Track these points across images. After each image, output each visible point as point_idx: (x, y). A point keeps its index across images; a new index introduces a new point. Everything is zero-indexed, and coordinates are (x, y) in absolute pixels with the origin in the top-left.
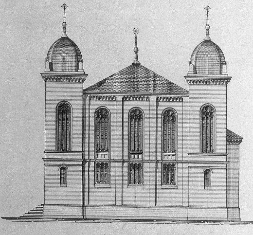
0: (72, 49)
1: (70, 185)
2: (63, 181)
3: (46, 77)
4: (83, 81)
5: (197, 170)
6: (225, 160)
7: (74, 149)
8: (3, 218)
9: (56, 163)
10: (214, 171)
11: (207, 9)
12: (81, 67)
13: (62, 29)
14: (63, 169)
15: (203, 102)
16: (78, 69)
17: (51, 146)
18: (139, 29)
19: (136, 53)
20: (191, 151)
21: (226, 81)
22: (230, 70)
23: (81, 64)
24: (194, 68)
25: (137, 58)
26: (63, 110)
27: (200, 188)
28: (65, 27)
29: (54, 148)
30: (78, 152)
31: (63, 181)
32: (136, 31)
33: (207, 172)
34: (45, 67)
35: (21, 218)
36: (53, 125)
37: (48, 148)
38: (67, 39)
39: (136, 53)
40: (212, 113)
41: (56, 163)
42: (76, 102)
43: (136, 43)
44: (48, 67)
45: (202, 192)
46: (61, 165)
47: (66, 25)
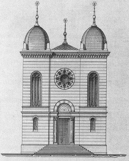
0: (99, 33)
1: (41, 131)
2: (35, 127)
3: (24, 55)
4: (107, 56)
5: (86, 119)
6: (48, 111)
7: (100, 105)
8: (2, 154)
9: (30, 115)
10: (40, 119)
11: (94, 4)
12: (105, 47)
13: (92, 20)
14: (35, 120)
15: (33, 70)
16: (46, 48)
17: (27, 103)
18: (68, 19)
19: (65, 36)
20: (81, 105)
21: (105, 55)
22: (108, 47)
23: (105, 45)
24: (27, 46)
25: (65, 40)
26: (36, 77)
27: (87, 131)
28: (37, 19)
29: (29, 105)
30: (46, 107)
31: (35, 127)
32: (65, 21)
33: (93, 120)
34: (22, 47)
35: (37, 154)
36: (85, 88)
37: (24, 105)
38: (39, 27)
39: (65, 36)
40: (96, 78)
41: (30, 115)
42: (102, 72)
43: (65, 29)
44: (25, 47)
45: (89, 134)
46: (92, 116)
47: (95, 17)
